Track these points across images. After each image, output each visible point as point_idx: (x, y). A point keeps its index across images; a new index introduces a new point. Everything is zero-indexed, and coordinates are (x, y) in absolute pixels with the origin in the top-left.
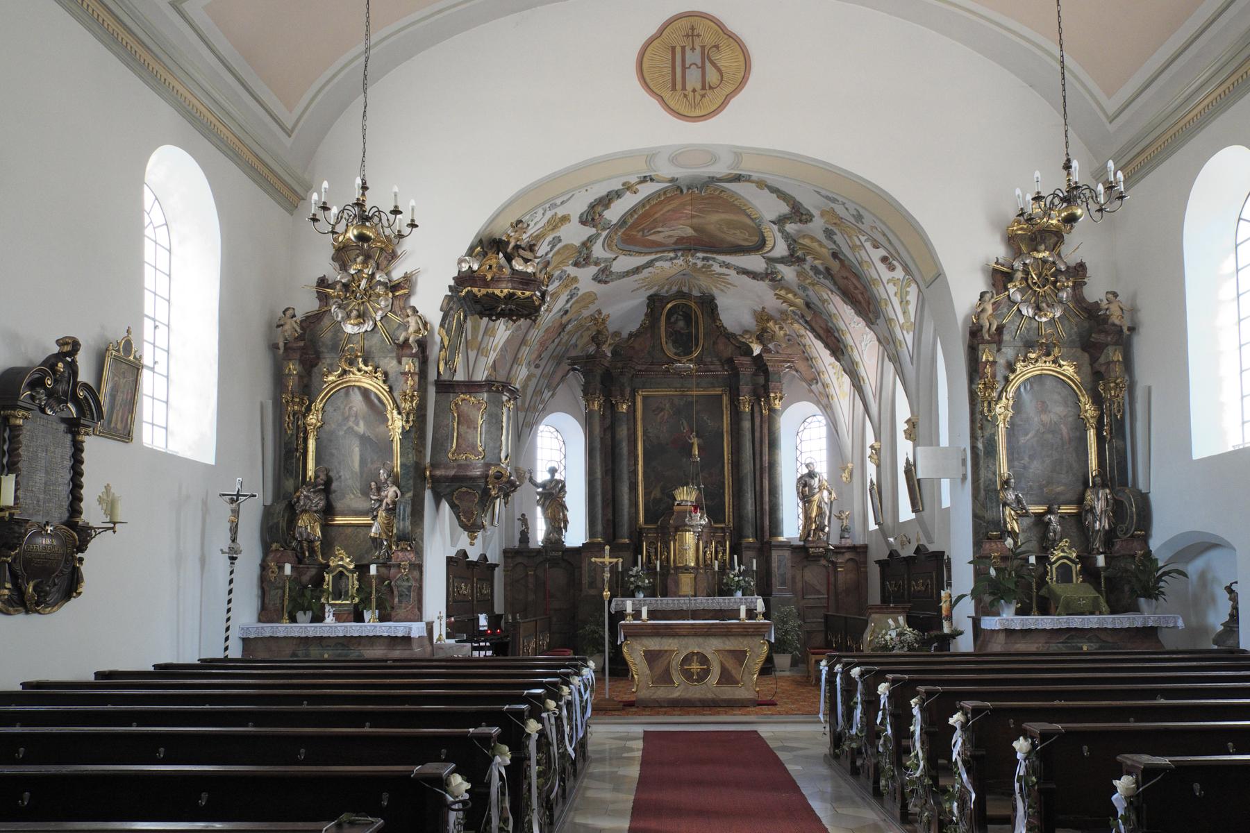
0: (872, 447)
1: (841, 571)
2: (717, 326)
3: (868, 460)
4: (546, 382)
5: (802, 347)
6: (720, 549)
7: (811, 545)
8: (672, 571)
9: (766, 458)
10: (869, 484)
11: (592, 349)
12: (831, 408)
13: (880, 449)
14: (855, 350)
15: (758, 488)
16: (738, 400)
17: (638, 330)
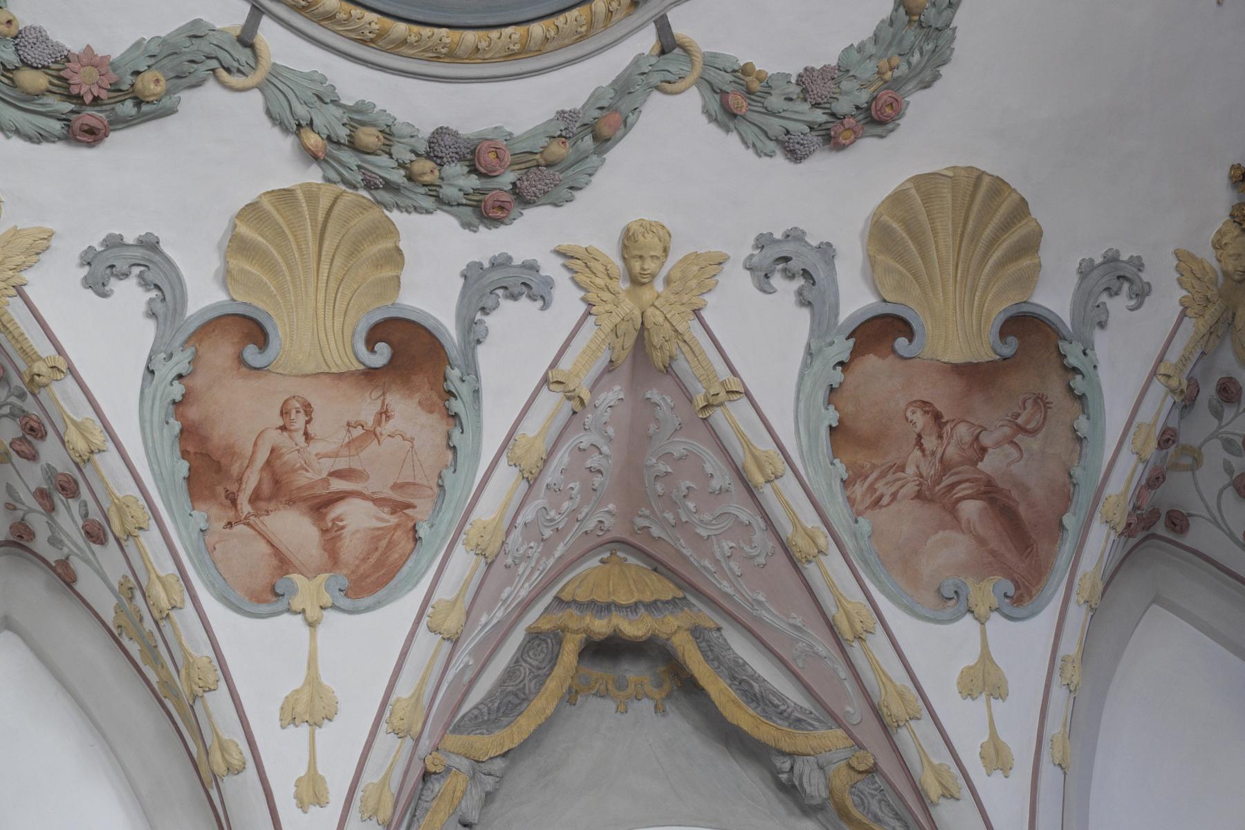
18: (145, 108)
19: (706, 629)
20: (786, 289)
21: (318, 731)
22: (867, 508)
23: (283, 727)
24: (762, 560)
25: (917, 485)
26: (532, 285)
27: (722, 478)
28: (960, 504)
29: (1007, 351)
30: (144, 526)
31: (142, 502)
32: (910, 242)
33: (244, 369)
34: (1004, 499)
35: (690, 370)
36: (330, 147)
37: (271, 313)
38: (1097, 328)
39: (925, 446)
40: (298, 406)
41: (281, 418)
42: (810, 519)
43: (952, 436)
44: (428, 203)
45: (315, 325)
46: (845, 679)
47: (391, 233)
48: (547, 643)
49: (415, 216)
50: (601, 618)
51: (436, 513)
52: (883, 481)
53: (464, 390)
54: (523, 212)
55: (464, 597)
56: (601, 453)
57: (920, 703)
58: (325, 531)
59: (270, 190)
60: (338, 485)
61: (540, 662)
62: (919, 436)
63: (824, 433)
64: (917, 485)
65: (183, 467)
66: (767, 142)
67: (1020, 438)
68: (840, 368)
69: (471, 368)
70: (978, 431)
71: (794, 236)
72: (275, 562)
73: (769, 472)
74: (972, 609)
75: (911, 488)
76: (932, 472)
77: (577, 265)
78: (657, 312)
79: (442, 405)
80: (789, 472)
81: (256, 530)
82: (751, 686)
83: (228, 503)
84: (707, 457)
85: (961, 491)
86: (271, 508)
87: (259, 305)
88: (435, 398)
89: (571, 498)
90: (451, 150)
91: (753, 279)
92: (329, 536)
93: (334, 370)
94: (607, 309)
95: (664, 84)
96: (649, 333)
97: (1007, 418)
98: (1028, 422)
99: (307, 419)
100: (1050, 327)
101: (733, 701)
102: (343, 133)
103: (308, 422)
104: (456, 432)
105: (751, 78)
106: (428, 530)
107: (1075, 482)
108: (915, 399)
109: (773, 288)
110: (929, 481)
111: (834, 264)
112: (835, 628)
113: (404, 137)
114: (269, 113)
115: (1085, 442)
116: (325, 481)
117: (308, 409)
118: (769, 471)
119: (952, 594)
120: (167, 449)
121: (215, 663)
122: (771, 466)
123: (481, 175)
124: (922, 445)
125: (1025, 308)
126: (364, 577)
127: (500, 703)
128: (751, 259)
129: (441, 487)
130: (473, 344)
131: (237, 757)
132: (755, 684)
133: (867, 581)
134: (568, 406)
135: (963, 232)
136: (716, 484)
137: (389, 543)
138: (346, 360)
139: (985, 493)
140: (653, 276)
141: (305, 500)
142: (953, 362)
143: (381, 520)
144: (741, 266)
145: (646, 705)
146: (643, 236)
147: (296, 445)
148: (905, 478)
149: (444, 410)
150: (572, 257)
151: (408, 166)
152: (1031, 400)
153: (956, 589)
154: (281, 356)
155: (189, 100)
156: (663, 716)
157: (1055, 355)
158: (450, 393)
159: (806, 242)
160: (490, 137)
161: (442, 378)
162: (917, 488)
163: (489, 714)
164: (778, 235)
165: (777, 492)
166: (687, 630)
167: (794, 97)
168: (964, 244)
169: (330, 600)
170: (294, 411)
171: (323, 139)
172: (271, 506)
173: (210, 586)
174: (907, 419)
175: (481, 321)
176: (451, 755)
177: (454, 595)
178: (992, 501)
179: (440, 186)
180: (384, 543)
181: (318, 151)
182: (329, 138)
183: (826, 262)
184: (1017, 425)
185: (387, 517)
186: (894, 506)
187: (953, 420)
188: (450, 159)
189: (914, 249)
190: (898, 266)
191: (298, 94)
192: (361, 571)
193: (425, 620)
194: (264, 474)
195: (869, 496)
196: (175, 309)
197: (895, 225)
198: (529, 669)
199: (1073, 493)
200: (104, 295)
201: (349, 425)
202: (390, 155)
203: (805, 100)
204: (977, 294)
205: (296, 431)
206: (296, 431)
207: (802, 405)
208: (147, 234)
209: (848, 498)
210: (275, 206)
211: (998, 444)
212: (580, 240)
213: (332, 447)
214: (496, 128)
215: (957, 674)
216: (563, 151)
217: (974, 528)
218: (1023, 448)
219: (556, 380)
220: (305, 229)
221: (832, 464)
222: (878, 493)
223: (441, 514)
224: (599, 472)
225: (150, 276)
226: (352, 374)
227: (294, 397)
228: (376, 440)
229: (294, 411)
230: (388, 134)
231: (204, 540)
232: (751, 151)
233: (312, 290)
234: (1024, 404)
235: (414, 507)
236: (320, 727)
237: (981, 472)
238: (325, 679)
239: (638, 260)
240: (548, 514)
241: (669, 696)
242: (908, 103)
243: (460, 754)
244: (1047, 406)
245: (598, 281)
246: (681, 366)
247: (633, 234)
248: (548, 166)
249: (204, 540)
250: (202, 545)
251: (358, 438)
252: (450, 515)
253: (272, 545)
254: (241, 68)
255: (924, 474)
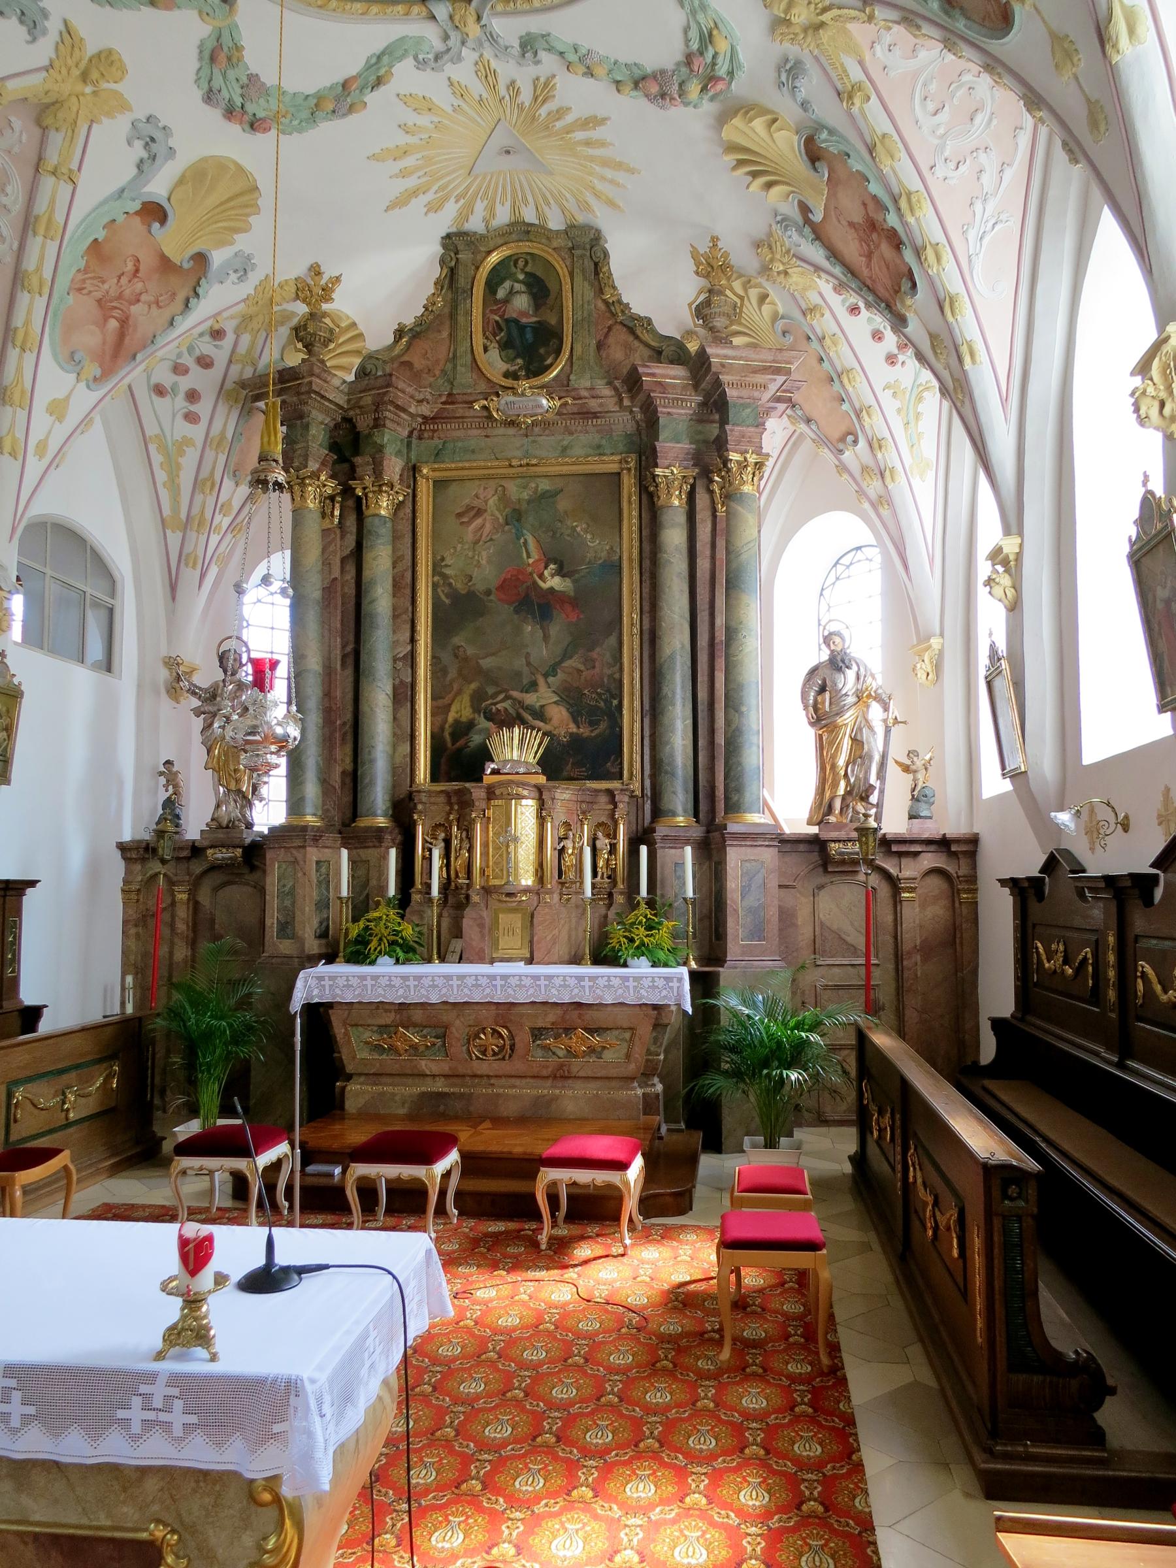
0: (996, 555)
1: (908, 900)
2: (606, 302)
3: (982, 592)
4: (222, 459)
5: (815, 344)
6: (603, 842)
7: (834, 835)
8: (475, 898)
9: (720, 621)
10: (983, 661)
11: (294, 359)
12: (890, 503)
13: (1019, 556)
14: (947, 256)
15: (702, 695)
16: (654, 477)
17: (420, 321)
20: (139, 151)
29: (186, 266)
67: (154, 306)
75: (98, 295)
178: (122, 327)
211: (145, 303)
212: (82, 28)
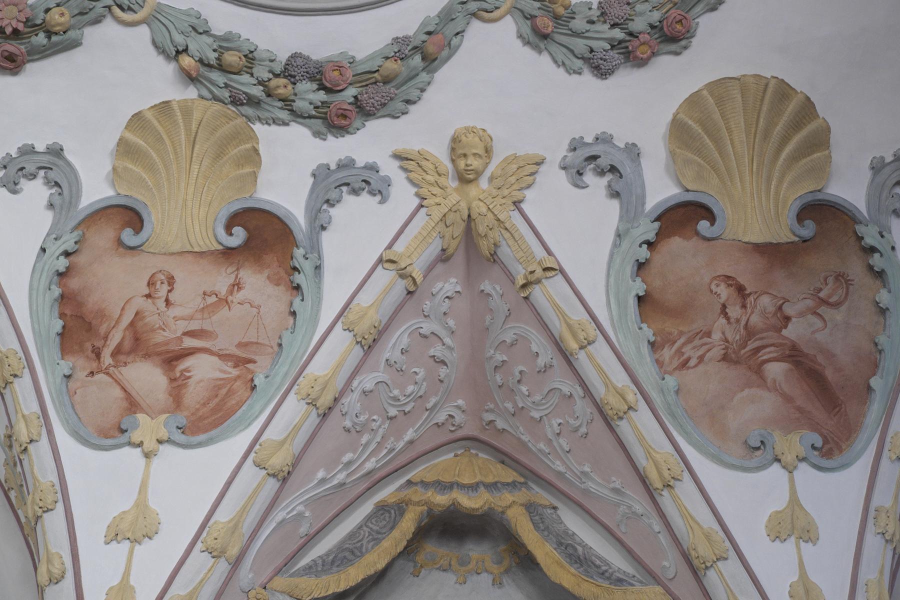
18: (54, 38)
19: (540, 505)
20: (597, 184)
21: (137, 547)
22: (675, 369)
23: (107, 543)
24: (583, 430)
25: (723, 349)
26: (371, 181)
27: (546, 354)
28: (765, 365)
30: (18, 373)
31: (21, 354)
32: (706, 137)
33: (121, 250)
34: (810, 363)
35: (511, 254)
36: (203, 70)
37: (148, 203)
38: (893, 217)
39: (730, 314)
40: (163, 277)
41: (148, 287)
42: (620, 378)
43: (756, 306)
44: (284, 115)
45: (184, 214)
46: (659, 532)
47: (252, 138)
48: (390, 513)
49: (274, 128)
50: (443, 494)
51: (273, 366)
52: (690, 346)
53: (307, 266)
54: (366, 123)
55: (293, 439)
56: (444, 345)
57: (728, 544)
58: (172, 380)
59: (153, 105)
60: (189, 343)
61: (381, 528)
62: (724, 306)
63: (632, 302)
64: (723, 349)
65: (58, 325)
66: (575, 60)
68: (646, 245)
69: (315, 247)
70: (781, 302)
71: (604, 139)
72: (125, 404)
73: (582, 337)
74: (779, 457)
75: (717, 352)
76: (738, 337)
77: (411, 165)
78: (481, 204)
79: (288, 279)
80: (601, 338)
81: (113, 378)
82: (576, 550)
83: (93, 356)
84: (533, 336)
85: (764, 355)
86: (129, 361)
87: (138, 196)
88: (283, 273)
89: (416, 383)
90: (302, 69)
91: (567, 177)
92: (175, 384)
93: (196, 250)
94: (437, 201)
95: (482, 12)
96: (475, 224)
97: (809, 292)
98: (830, 296)
99: (169, 288)
100: (847, 215)
101: (557, 562)
102: (212, 56)
103: (169, 291)
104: (297, 301)
105: (557, 5)
106: (264, 379)
107: (880, 347)
108: (718, 274)
109: (585, 183)
110: (734, 345)
111: (640, 162)
112: (647, 481)
113: (264, 61)
114: (154, 43)
115: (888, 313)
116: (180, 339)
117: (171, 281)
118: (582, 336)
119: (758, 444)
120: (47, 310)
121: (58, 487)
122: (583, 333)
123: (329, 91)
124: (727, 313)
125: (820, 196)
126: (202, 419)
127: (335, 557)
128: (565, 159)
129: (280, 345)
130: (318, 229)
131: (58, 567)
132: (578, 547)
133: (675, 434)
134: (401, 285)
135: (756, 131)
136: (541, 362)
137: (229, 391)
138: (207, 241)
139: (790, 356)
140: (478, 174)
141: (159, 354)
142: (754, 242)
143: (225, 372)
144: (557, 166)
145: (486, 579)
146: (466, 136)
147: (158, 309)
148: (711, 343)
149: (290, 284)
150: (407, 159)
151: (267, 83)
152: (833, 277)
153: (762, 439)
154: (153, 238)
155: (91, 34)
156: (499, 588)
157: (853, 239)
158: (295, 269)
159: (614, 144)
160: (336, 60)
161: (290, 257)
162: (723, 352)
163: (323, 565)
164: (589, 139)
165: (590, 357)
166: (522, 505)
167: (595, 19)
168: (757, 140)
169: (167, 434)
170: (159, 283)
171: (196, 61)
172: (130, 359)
173: (66, 422)
174: (711, 291)
175: (325, 211)
176: (275, 592)
177: (282, 437)
179: (294, 101)
180: (224, 391)
181: (191, 70)
182: (201, 61)
183: (632, 160)
184: (819, 298)
185: (230, 370)
186: (701, 368)
187: (756, 292)
188: (302, 78)
189: (712, 147)
190: (699, 160)
191: (176, 25)
192: (200, 413)
193: (253, 455)
194: (127, 333)
195: (676, 358)
196: (70, 203)
197: (690, 122)
198: (369, 532)
199: (880, 359)
200: (14, 192)
201: (205, 294)
202: (252, 75)
203: (605, 22)
204: (773, 183)
205: (158, 298)
206: (158, 298)
207: (612, 280)
208: (54, 143)
209: (657, 361)
210: (157, 119)
211: (801, 315)
212: (413, 144)
213: (187, 312)
214: (341, 53)
215: (766, 518)
216: (396, 66)
217: (780, 386)
218: (826, 319)
219: (388, 258)
220: (179, 136)
221: (640, 328)
222: (685, 356)
223: (277, 367)
224: (443, 363)
225: (52, 175)
226: (212, 253)
227: (160, 271)
228: (227, 307)
229: (159, 283)
230: (250, 58)
231: (67, 386)
232: (562, 70)
233: (183, 185)
234: (825, 280)
235: (255, 362)
236: (140, 544)
237: (785, 338)
238: (153, 503)
239: (463, 158)
240: (391, 392)
241: (507, 571)
242: (697, 24)
243: (284, 592)
244: (849, 283)
245: (428, 178)
246: (506, 252)
247: (458, 136)
248: (385, 83)
249: (67, 386)
250: (64, 389)
251: (211, 304)
252: (285, 368)
253: (125, 391)
254: (131, 5)
255: (730, 339)
